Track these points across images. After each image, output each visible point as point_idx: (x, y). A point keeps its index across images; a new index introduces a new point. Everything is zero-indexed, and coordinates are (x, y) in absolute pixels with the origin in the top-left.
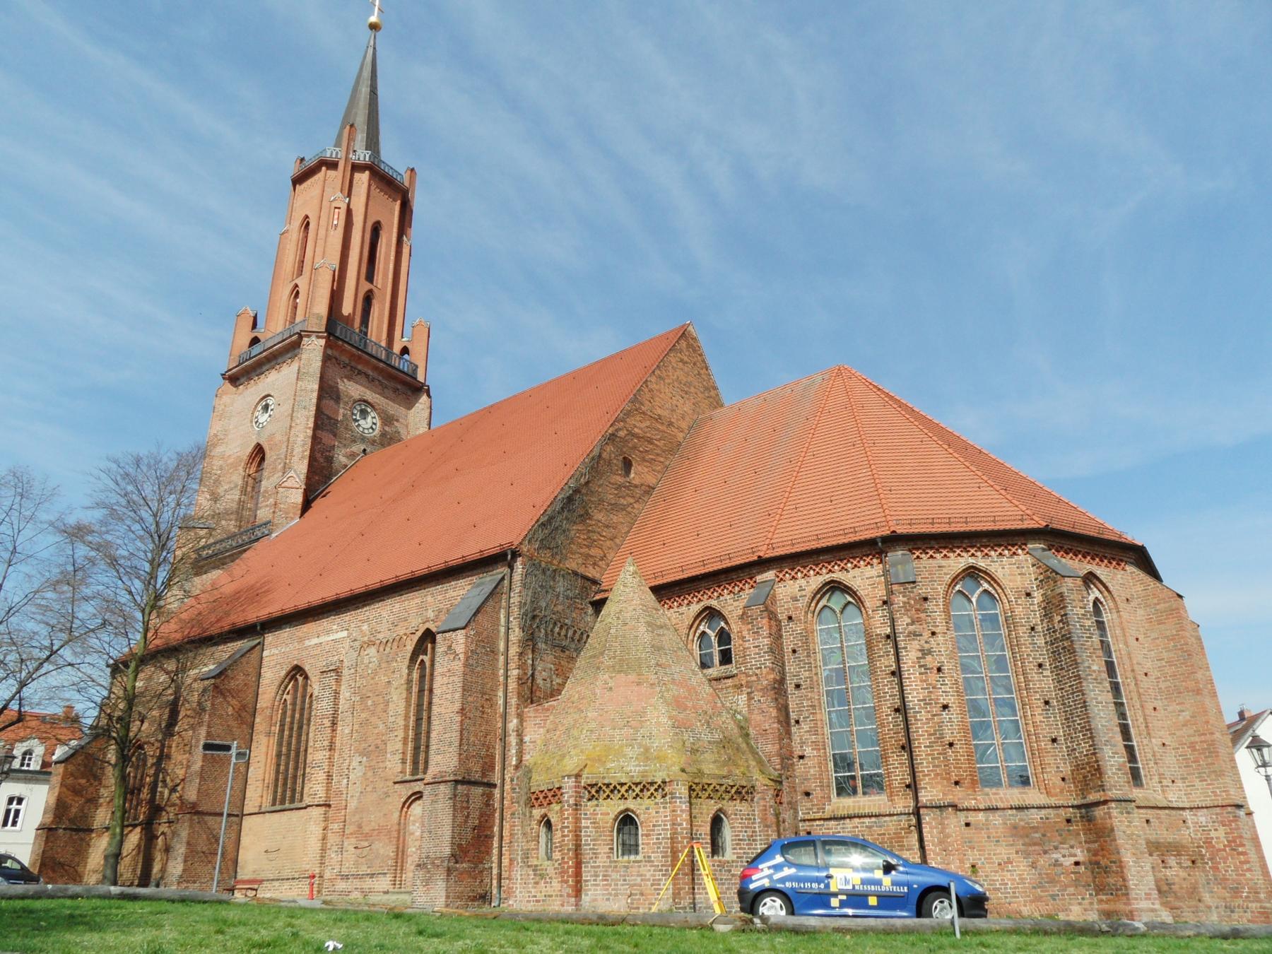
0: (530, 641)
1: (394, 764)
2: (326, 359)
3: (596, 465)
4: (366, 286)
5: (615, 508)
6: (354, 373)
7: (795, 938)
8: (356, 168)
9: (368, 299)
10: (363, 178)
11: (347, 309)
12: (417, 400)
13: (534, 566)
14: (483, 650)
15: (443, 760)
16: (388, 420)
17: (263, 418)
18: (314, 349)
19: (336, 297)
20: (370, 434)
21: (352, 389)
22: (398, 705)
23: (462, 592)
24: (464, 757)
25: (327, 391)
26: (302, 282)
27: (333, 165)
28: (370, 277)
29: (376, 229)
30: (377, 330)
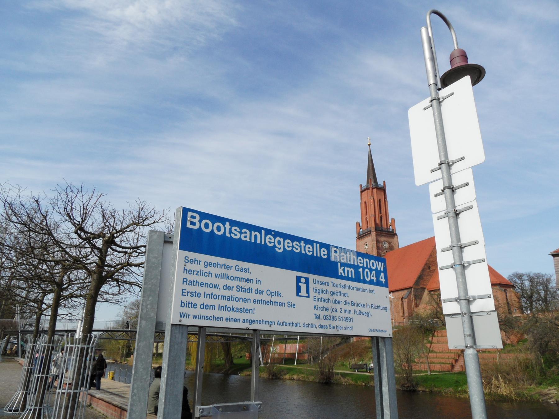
0: (415, 299)
1: (401, 314)
2: (376, 235)
3: (423, 270)
4: (380, 215)
5: (428, 275)
6: (382, 236)
7: (506, 305)
8: (373, 188)
9: (381, 217)
10: (375, 190)
11: (377, 221)
12: (393, 334)
13: (415, 289)
14: (409, 301)
15: (406, 314)
16: (389, 243)
17: (367, 247)
18: (374, 234)
19: (376, 224)
20: (387, 247)
21: (382, 239)
22: (400, 306)
23: (406, 292)
24: (409, 314)
25: (378, 242)
26: (368, 216)
27: (369, 189)
28: (381, 213)
29: (380, 201)
30: (384, 226)
